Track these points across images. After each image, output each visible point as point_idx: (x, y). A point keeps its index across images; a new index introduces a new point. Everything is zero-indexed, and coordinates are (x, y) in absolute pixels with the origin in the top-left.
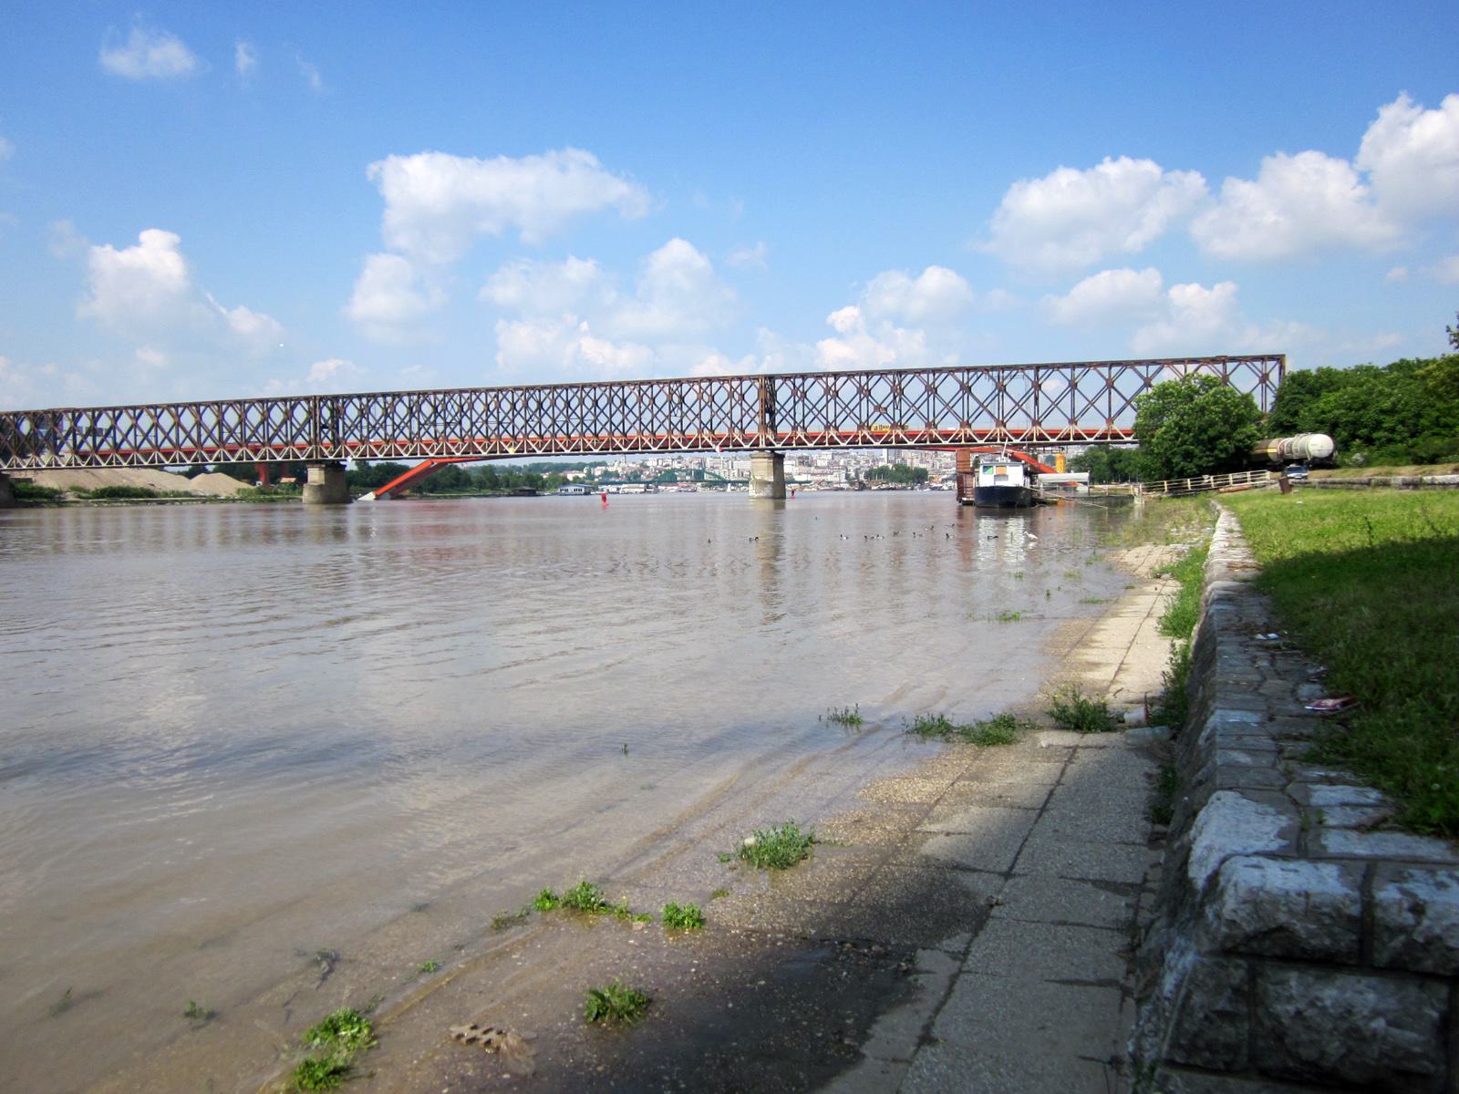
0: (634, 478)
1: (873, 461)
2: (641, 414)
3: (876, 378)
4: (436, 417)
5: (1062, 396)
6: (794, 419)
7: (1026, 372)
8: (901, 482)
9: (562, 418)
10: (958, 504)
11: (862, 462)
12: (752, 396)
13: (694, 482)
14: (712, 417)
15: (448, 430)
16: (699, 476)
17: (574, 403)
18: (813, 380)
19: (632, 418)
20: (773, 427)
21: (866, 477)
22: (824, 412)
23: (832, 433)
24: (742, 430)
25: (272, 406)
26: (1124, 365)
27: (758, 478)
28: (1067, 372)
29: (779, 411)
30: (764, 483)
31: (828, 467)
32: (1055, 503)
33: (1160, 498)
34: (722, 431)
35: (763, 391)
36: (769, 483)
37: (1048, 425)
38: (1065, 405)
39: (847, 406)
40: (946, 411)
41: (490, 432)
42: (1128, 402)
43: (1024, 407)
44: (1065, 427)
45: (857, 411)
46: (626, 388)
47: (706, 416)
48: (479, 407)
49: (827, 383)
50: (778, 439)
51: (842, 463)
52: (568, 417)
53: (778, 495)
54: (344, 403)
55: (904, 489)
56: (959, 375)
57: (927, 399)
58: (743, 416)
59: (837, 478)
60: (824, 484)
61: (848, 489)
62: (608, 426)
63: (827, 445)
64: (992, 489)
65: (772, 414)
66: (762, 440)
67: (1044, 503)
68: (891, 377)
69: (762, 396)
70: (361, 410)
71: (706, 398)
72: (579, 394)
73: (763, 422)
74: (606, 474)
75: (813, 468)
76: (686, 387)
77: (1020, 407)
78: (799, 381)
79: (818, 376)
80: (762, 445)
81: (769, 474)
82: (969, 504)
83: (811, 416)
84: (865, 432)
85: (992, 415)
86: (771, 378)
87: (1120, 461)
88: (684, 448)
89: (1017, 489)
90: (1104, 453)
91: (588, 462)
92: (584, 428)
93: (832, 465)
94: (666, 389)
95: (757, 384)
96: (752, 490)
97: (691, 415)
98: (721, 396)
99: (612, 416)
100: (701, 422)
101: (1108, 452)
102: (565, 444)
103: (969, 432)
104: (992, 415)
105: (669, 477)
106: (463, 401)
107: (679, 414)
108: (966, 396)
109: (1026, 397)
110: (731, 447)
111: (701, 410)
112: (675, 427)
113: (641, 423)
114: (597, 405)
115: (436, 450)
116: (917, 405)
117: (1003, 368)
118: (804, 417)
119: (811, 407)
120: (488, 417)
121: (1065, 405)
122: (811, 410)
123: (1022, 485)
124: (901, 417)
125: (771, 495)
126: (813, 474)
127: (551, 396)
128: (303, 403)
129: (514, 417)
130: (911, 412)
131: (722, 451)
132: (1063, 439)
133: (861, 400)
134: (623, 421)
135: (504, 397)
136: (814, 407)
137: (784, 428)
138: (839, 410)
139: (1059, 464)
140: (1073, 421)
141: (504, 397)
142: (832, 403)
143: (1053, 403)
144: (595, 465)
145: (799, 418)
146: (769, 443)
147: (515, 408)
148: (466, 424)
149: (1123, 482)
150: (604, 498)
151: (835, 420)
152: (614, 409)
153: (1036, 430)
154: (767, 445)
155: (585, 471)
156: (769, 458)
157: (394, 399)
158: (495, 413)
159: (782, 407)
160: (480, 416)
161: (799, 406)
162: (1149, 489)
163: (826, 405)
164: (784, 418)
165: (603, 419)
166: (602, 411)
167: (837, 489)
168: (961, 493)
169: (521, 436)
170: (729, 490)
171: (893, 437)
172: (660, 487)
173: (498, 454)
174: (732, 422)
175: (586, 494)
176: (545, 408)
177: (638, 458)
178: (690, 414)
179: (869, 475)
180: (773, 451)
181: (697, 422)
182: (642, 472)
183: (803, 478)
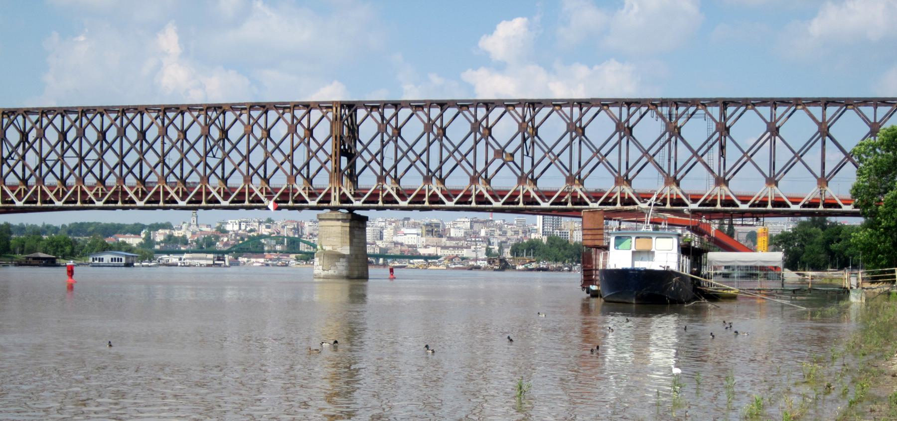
0: (206, 246)
1: (524, 232)
2: (249, 152)
3: (546, 111)
5: (757, 147)
6: (427, 166)
7: (709, 109)
8: (556, 260)
9: (93, 156)
10: (585, 295)
11: (509, 234)
12: (322, 132)
13: (288, 253)
14: (310, 159)
16: (293, 245)
17: (111, 135)
18: (455, 110)
19: (235, 157)
20: (353, 177)
21: (512, 253)
22: (470, 158)
23: (481, 188)
24: (309, 180)
26: (846, 103)
27: (328, 248)
28: (765, 111)
29: (360, 154)
30: (336, 257)
31: (465, 239)
32: (733, 298)
33: (889, 294)
34: (279, 181)
35: (337, 125)
36: (343, 256)
37: (737, 187)
38: (762, 157)
39: (456, 149)
40: (596, 160)
41: (28, 173)
42: (848, 156)
43: (705, 158)
44: (759, 189)
45: (565, 158)
46: (187, 114)
49: (475, 116)
50: (357, 195)
51: (483, 233)
53: (356, 273)
55: (559, 269)
56: (615, 110)
57: (570, 144)
59: (477, 253)
60: (456, 260)
61: (485, 269)
62: (200, 168)
63: (427, 204)
64: (624, 273)
65: (351, 156)
66: (335, 195)
67: (714, 297)
68: (519, 110)
69: (337, 132)
71: (301, 131)
73: (338, 170)
74: (170, 239)
75: (444, 240)
76: (230, 116)
77: (800, 158)
78: (481, 112)
79: (463, 106)
80: (335, 203)
81: (343, 243)
82: (595, 294)
83: (451, 163)
84: (529, 188)
85: (660, 168)
86: (352, 106)
87: (839, 240)
89: (665, 275)
90: (819, 230)
91: (147, 223)
92: (125, 170)
93: (471, 235)
94: (288, 116)
95: (330, 115)
96: (318, 267)
97: (235, 156)
98: (280, 131)
100: (293, 166)
101: (824, 228)
102: (136, 193)
103: (628, 191)
104: (660, 168)
107: (220, 154)
108: (624, 141)
109: (708, 145)
110: (290, 204)
111: (293, 149)
113: (249, 165)
114: (144, 138)
116: (603, 152)
117: (677, 103)
118: (442, 163)
119: (451, 149)
121: (762, 157)
122: (405, 154)
123: (674, 267)
124: (534, 166)
125: (345, 273)
126: (445, 247)
127: (118, 122)
129: (64, 151)
130: (546, 161)
131: (279, 209)
132: (759, 205)
135: (51, 122)
136: (411, 148)
137: (368, 181)
138: (445, 154)
139: (762, 241)
140: (772, 181)
141: (51, 122)
142: (482, 145)
143: (745, 154)
144: (156, 227)
145: (388, 164)
146: (344, 199)
147: (65, 139)
149: (841, 268)
150: (392, 270)
151: (486, 170)
153: (721, 192)
154: (342, 202)
155: (143, 235)
156: (343, 220)
159: (365, 148)
161: (435, 147)
162: (874, 280)
163: (474, 148)
164: (413, 164)
165: (193, 157)
167: (472, 268)
168: (588, 279)
169: (32, 181)
171: (521, 196)
172: (241, 259)
173: (39, 204)
175: (128, 265)
176: (150, 141)
179: (516, 250)
180: (351, 210)
181: (287, 166)
182: (217, 238)
183: (431, 251)
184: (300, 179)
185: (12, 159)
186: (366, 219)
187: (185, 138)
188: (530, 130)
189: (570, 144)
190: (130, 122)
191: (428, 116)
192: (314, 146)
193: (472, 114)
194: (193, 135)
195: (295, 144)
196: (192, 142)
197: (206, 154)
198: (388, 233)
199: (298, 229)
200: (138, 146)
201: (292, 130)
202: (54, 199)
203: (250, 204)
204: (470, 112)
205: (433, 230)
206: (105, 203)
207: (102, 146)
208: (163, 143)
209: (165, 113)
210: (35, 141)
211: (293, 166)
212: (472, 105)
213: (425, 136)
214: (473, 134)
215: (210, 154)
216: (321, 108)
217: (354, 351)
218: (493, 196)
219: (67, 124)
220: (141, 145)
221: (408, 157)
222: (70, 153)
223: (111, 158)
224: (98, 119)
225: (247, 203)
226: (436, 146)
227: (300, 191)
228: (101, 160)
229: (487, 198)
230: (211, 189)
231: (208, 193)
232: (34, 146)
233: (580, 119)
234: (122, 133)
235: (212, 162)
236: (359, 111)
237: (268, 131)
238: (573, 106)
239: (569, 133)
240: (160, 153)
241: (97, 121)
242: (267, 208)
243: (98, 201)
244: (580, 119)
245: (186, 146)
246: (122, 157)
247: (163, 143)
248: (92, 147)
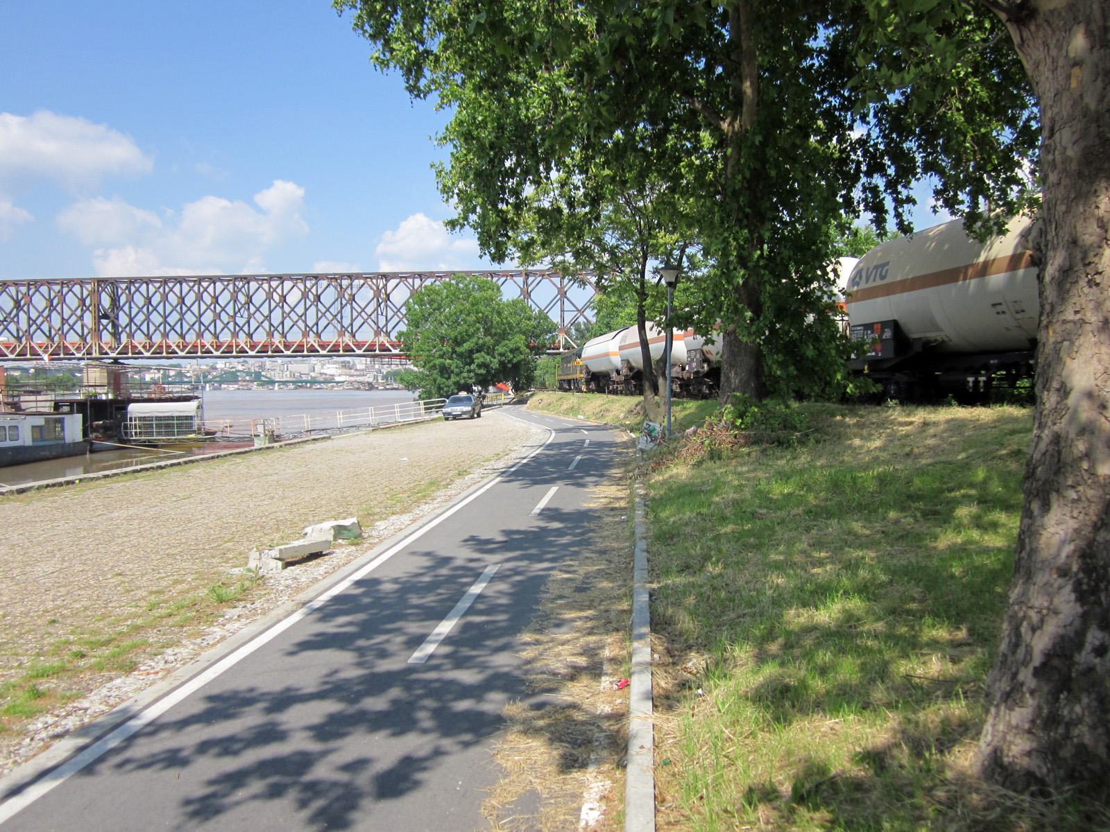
4: (51, 312)
6: (341, 323)
9: (141, 317)
15: (66, 327)
16: (257, 377)
34: (260, 337)
39: (363, 310)
46: (218, 284)
47: (276, 317)
48: (72, 301)
52: (182, 315)
58: (318, 319)
62: (196, 327)
71: (276, 297)
72: (196, 288)
76: (254, 285)
88: (251, 353)
92: (168, 328)
94: (231, 287)
98: (294, 297)
99: (201, 316)
100: (271, 325)
105: (231, 377)
106: (53, 295)
107: (246, 315)
111: (271, 312)
112: (241, 329)
114: (183, 302)
115: (50, 350)
118: (353, 320)
122: (359, 314)
127: (161, 290)
134: (214, 321)
135: (137, 290)
138: (355, 314)
145: (346, 322)
148: (56, 320)
152: (203, 307)
157: (29, 289)
160: (73, 313)
164: (295, 323)
165: (190, 318)
166: (189, 309)
170: (276, 388)
172: (223, 386)
174: (306, 325)
177: (210, 361)
178: (328, 314)
181: (266, 324)
182: (209, 373)
184: (241, 334)
187: (217, 302)
188: (383, 296)
194: (223, 300)
197: (235, 314)
198: (318, 368)
199: (262, 367)
200: (178, 308)
201: (269, 297)
202: (143, 350)
205: (345, 365)
207: (148, 309)
209: (200, 284)
210: (124, 305)
211: (271, 325)
212: (410, 277)
215: (239, 315)
216: (257, 280)
217: (340, 430)
218: (392, 346)
219: (85, 293)
220: (181, 308)
223: (156, 318)
224: (77, 289)
225: (234, 354)
226: (347, 309)
227: (242, 345)
228: (148, 319)
230: (171, 344)
231: (203, 346)
234: (165, 298)
235: (241, 321)
237: (217, 298)
238: (414, 278)
241: (177, 289)
242: (42, 359)
245: (218, 309)
246: (165, 317)
248: (140, 310)
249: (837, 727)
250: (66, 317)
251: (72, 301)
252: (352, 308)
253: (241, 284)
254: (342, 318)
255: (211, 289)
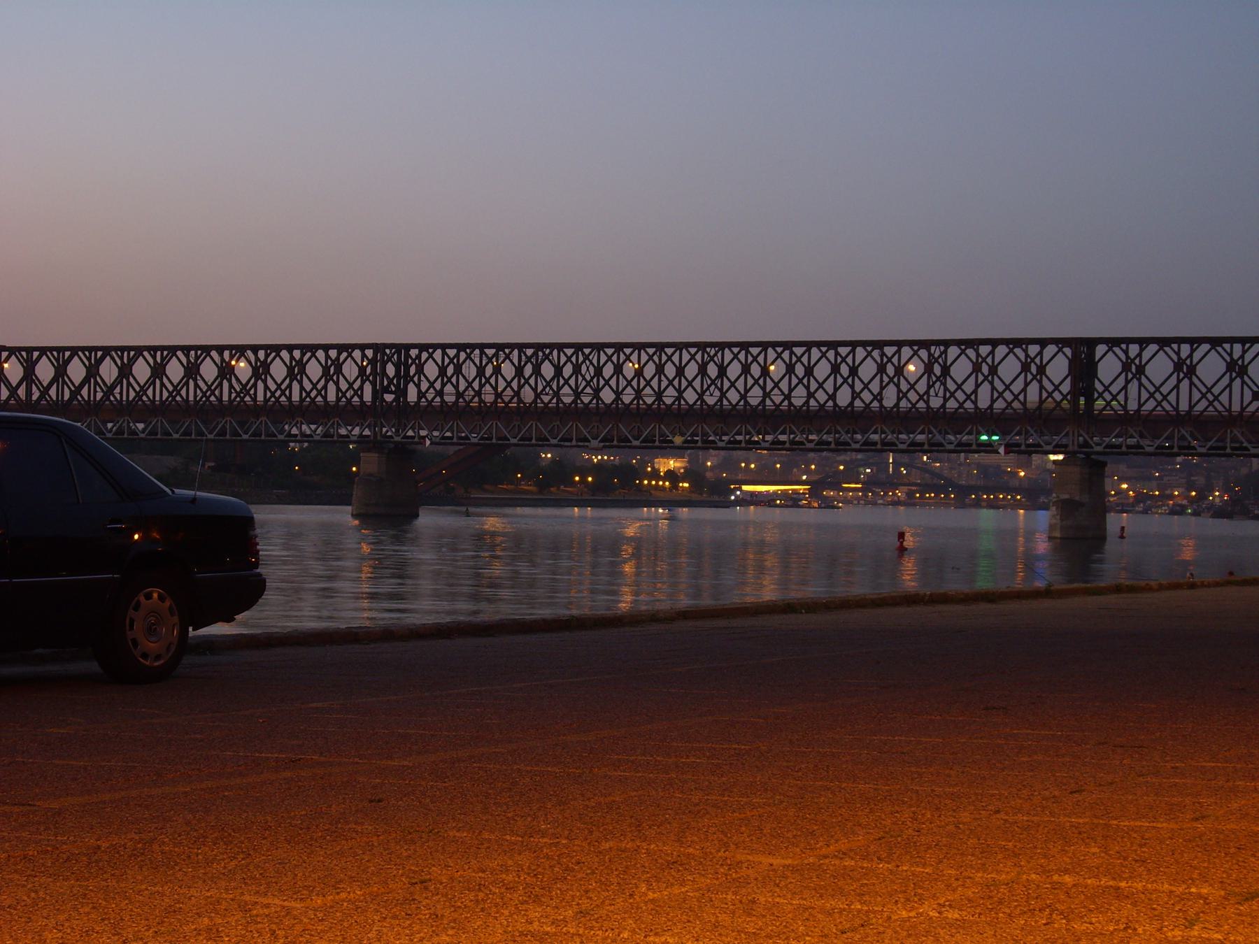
4: (327, 382)
25: (71, 358)
46: (814, 351)
49: (1178, 353)
54: (197, 358)
57: (1230, 385)
70: (290, 369)
78: (1134, 349)
86: (1091, 343)
98: (822, 370)
120: (443, 385)
128: (179, 353)
133: (1179, 381)
141: (469, 357)
142: (1185, 384)
158: (493, 381)
161: (1133, 387)
180: (1088, 455)
185: (547, 394)
186: (1104, 464)
189: (1230, 385)
190: (669, 358)
191: (1126, 352)
192: (904, 386)
193: (1174, 351)
195: (1028, 380)
196: (648, 379)
203: (382, 439)
204: (1121, 349)
206: (520, 440)
208: (660, 381)
210: (414, 375)
213: (1123, 375)
214: (833, 375)
215: (708, 393)
221: (1214, 395)
222: (566, 390)
229: (273, 432)
232: (530, 381)
233: (1242, 357)
236: (34, 353)
239: (1228, 374)
240: (699, 391)
243: (209, 433)
244: (1242, 357)
247: (660, 381)
249: (920, 791)
250: (423, 389)
251: (350, 370)
252: (1141, 385)
253: (713, 352)
254: (1126, 399)
255: (676, 358)
